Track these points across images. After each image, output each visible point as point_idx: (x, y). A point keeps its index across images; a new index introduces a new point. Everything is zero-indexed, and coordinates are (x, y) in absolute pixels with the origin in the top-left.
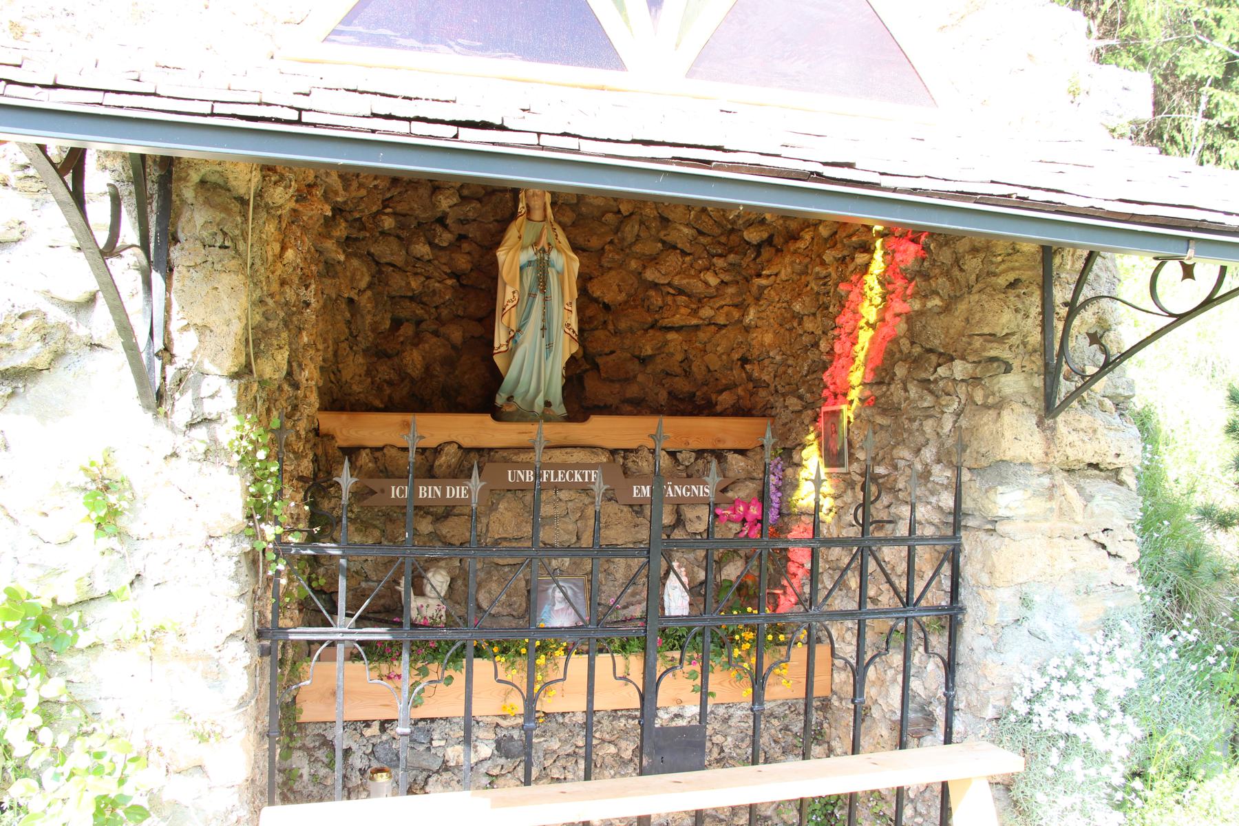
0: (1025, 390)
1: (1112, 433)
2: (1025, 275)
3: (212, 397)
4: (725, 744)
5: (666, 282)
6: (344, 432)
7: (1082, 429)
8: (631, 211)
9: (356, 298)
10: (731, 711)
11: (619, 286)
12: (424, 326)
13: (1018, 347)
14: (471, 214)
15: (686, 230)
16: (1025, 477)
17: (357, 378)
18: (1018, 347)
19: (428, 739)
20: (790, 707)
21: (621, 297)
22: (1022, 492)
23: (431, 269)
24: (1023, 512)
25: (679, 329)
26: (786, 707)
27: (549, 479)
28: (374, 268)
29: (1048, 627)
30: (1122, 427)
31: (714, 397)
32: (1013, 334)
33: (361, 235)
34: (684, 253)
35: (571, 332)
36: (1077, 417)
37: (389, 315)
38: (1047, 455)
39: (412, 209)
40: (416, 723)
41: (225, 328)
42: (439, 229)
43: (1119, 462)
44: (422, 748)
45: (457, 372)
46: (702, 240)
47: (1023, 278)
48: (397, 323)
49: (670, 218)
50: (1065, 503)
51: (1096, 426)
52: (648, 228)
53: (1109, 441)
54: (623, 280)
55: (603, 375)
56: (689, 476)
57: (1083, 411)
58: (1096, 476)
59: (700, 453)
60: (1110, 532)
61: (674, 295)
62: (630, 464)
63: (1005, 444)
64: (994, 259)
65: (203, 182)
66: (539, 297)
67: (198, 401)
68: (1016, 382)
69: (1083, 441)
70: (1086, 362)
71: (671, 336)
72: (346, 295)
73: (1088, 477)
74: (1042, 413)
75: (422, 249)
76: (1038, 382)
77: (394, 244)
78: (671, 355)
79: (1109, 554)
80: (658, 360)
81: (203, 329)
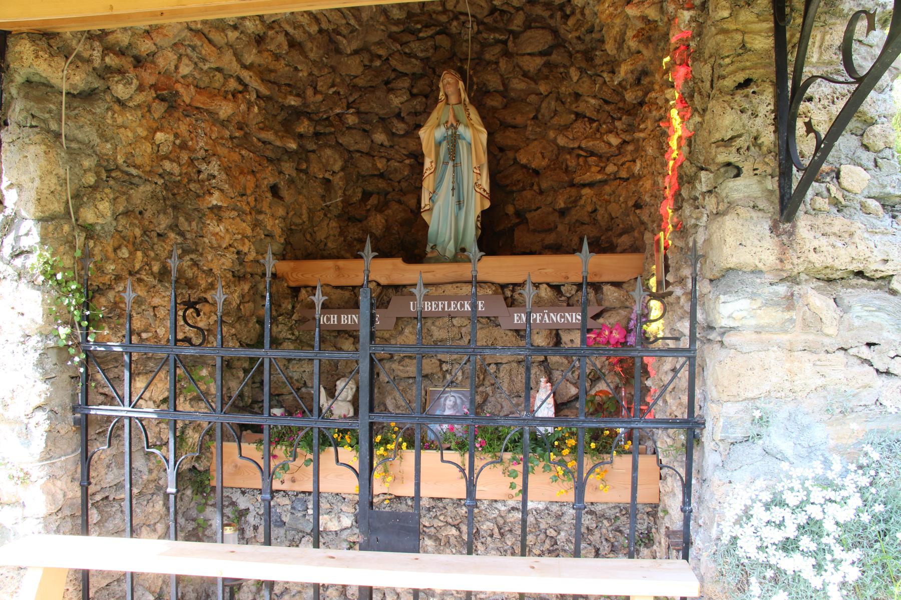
0: (759, 194)
1: (877, 237)
2: (756, 74)
3: (27, 235)
4: (559, 537)
5: (576, 145)
6: (294, 275)
7: (835, 234)
8: (549, 90)
9: (331, 178)
10: (565, 509)
11: (542, 153)
12: (389, 197)
13: (748, 149)
14: (418, 107)
15: (593, 101)
16: (753, 284)
17: (332, 238)
18: (748, 149)
19: (304, 508)
20: (621, 510)
21: (544, 163)
22: (749, 301)
23: (392, 152)
24: (753, 322)
25: (591, 185)
26: (618, 510)
27: (443, 308)
28: (346, 156)
29: (785, 446)
30: (890, 230)
31: (614, 240)
32: (740, 136)
33: (328, 130)
34: (592, 121)
35: (482, 191)
36: (828, 221)
37: (360, 190)
38: (781, 261)
39: (372, 108)
40: (297, 495)
41: (30, 184)
42: (395, 121)
43: (888, 269)
44: (300, 514)
45: (413, 231)
46: (607, 108)
47: (755, 77)
48: (366, 195)
49: (580, 92)
50: (808, 313)
51: (853, 230)
52: (563, 103)
53: (872, 245)
54: (544, 148)
55: (532, 227)
56: (568, 305)
57: (839, 215)
58: (863, 286)
59: (579, 286)
60: (876, 347)
61: (586, 157)
62: (516, 296)
63: (726, 250)
64: (722, 62)
65: (29, 82)
66: (451, 164)
67: (17, 238)
68: (746, 186)
69: (834, 246)
70: (843, 161)
71: (586, 191)
72: (321, 176)
73: (853, 287)
74: (777, 217)
75: (380, 137)
76: (772, 184)
77: (358, 135)
78: (583, 206)
79: (877, 370)
80: (573, 212)
81: (20, 187)
